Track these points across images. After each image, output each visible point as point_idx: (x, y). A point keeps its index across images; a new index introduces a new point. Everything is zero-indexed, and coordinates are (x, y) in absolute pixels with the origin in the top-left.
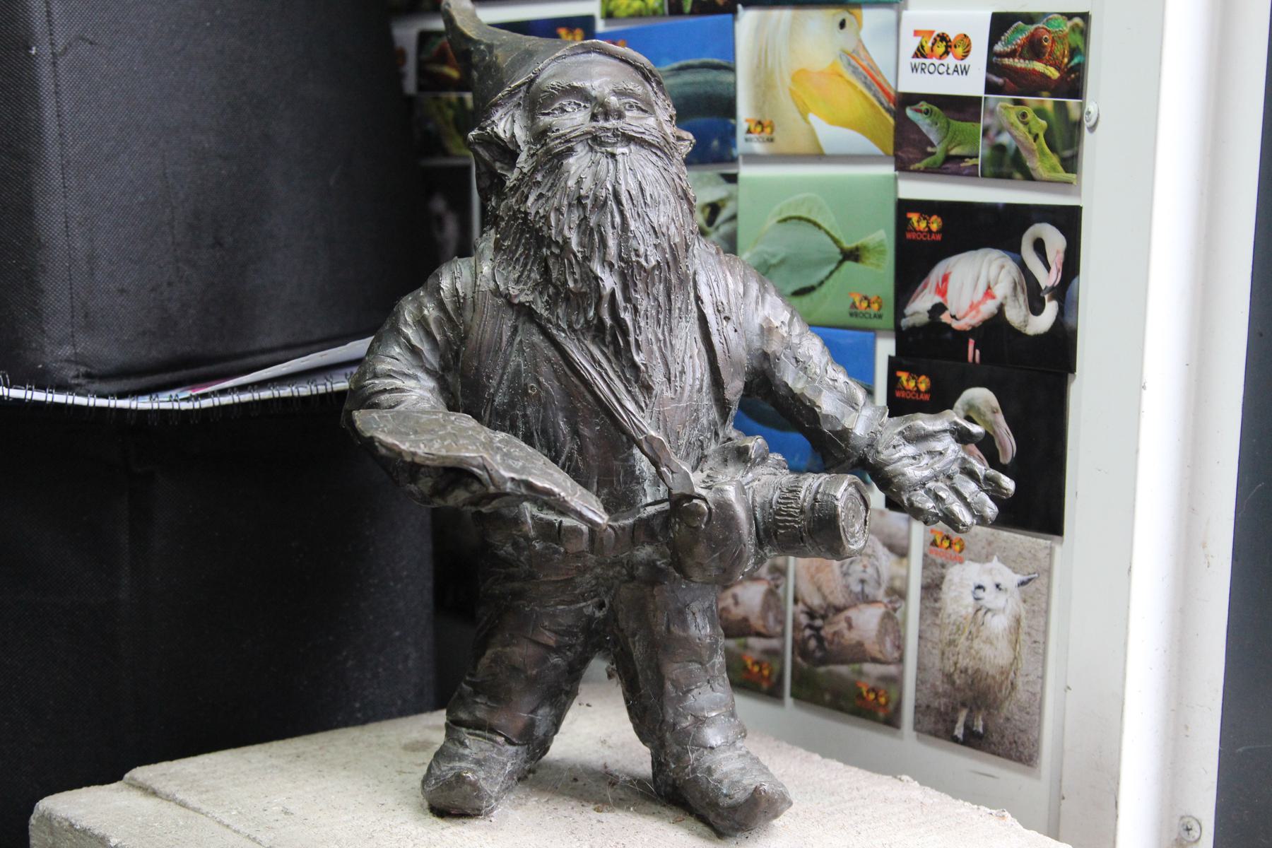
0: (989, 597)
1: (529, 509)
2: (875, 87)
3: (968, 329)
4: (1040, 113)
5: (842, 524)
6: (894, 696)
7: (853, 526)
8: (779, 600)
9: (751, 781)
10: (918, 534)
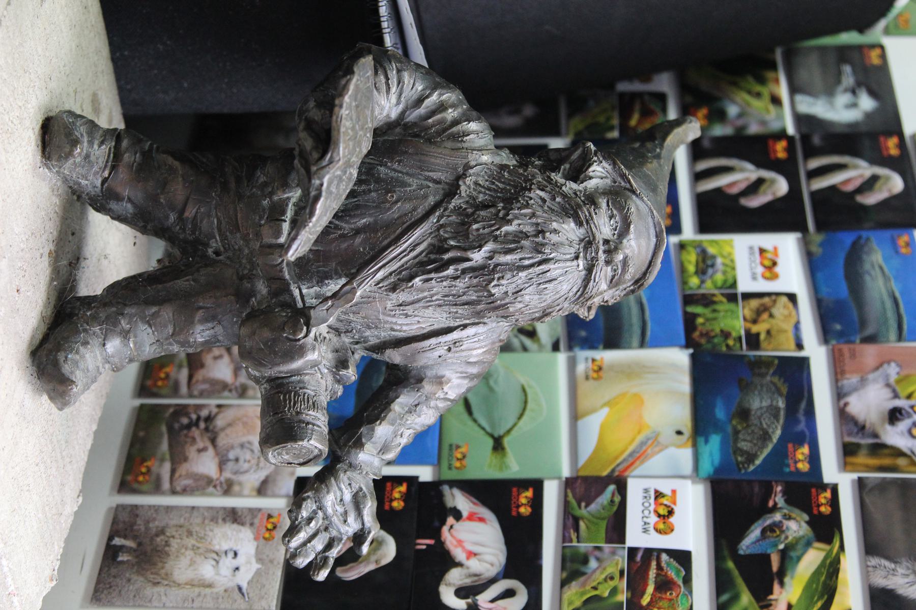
0: (227, 563)
1: (295, 195)
2: (631, 460)
3: (442, 539)
4: (614, 591)
5: (289, 445)
6: (145, 487)
7: (287, 454)
8: (219, 392)
9: (78, 376)
10: (278, 503)
